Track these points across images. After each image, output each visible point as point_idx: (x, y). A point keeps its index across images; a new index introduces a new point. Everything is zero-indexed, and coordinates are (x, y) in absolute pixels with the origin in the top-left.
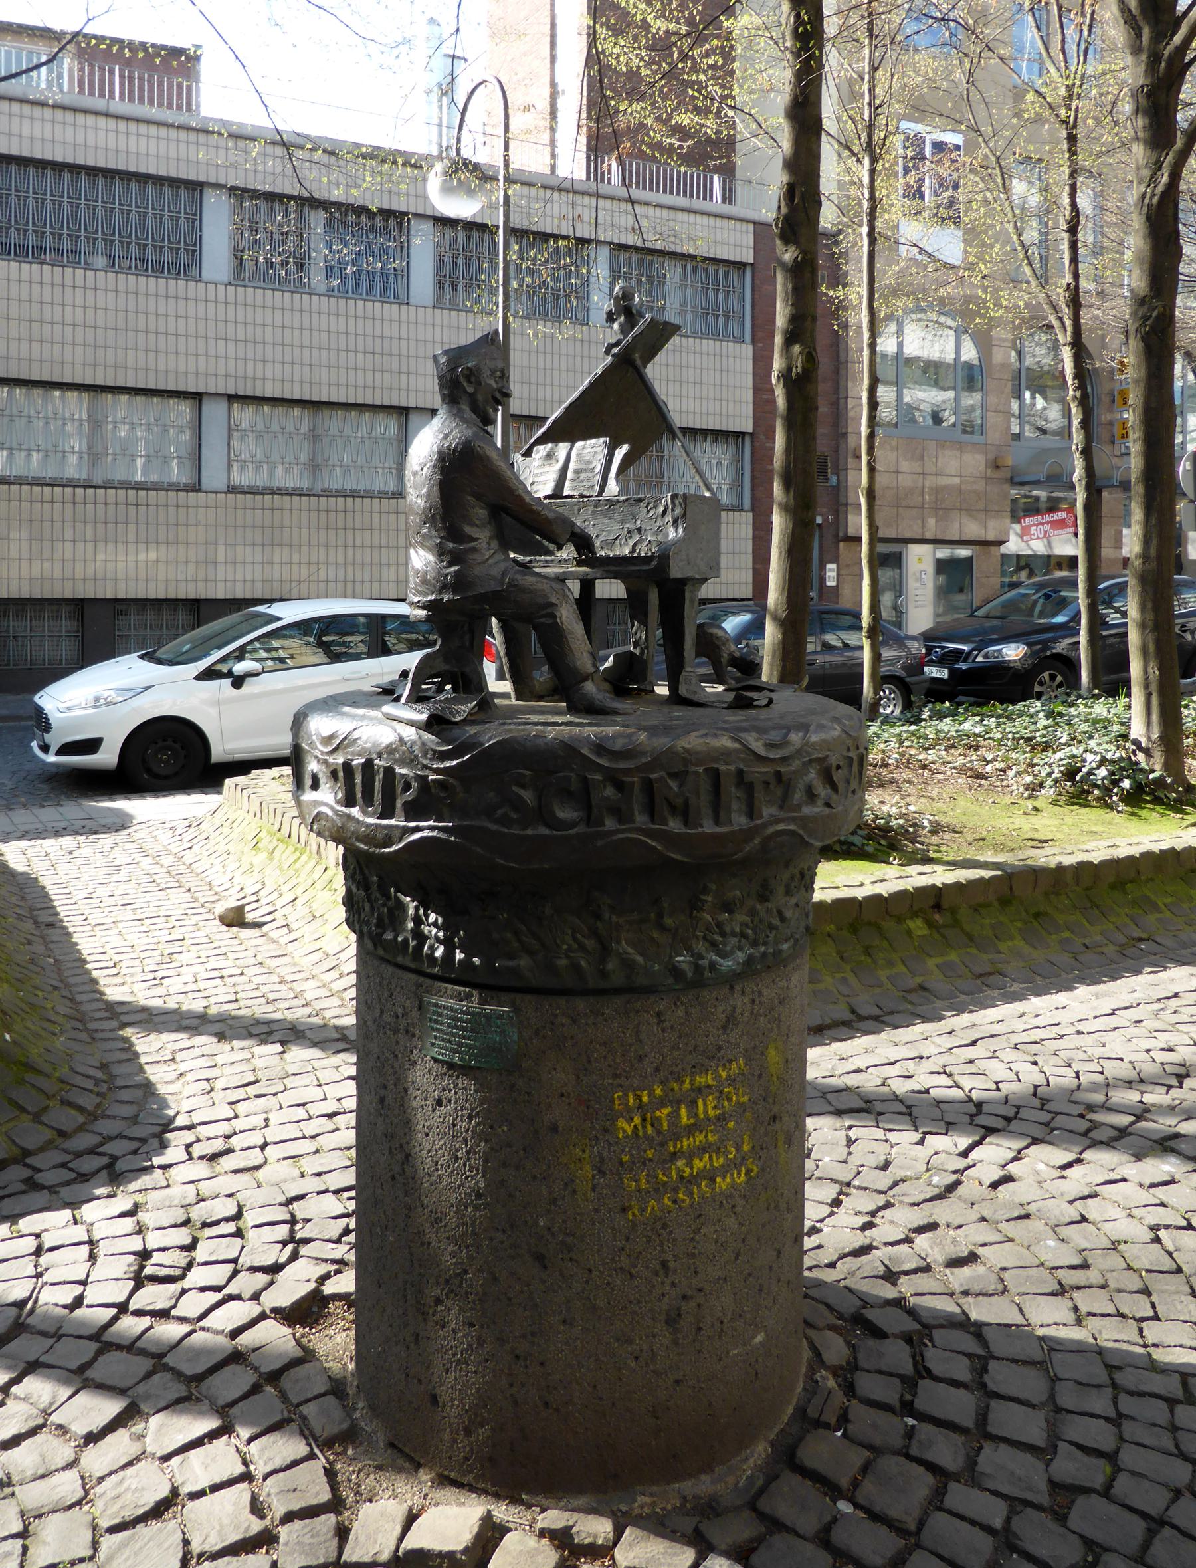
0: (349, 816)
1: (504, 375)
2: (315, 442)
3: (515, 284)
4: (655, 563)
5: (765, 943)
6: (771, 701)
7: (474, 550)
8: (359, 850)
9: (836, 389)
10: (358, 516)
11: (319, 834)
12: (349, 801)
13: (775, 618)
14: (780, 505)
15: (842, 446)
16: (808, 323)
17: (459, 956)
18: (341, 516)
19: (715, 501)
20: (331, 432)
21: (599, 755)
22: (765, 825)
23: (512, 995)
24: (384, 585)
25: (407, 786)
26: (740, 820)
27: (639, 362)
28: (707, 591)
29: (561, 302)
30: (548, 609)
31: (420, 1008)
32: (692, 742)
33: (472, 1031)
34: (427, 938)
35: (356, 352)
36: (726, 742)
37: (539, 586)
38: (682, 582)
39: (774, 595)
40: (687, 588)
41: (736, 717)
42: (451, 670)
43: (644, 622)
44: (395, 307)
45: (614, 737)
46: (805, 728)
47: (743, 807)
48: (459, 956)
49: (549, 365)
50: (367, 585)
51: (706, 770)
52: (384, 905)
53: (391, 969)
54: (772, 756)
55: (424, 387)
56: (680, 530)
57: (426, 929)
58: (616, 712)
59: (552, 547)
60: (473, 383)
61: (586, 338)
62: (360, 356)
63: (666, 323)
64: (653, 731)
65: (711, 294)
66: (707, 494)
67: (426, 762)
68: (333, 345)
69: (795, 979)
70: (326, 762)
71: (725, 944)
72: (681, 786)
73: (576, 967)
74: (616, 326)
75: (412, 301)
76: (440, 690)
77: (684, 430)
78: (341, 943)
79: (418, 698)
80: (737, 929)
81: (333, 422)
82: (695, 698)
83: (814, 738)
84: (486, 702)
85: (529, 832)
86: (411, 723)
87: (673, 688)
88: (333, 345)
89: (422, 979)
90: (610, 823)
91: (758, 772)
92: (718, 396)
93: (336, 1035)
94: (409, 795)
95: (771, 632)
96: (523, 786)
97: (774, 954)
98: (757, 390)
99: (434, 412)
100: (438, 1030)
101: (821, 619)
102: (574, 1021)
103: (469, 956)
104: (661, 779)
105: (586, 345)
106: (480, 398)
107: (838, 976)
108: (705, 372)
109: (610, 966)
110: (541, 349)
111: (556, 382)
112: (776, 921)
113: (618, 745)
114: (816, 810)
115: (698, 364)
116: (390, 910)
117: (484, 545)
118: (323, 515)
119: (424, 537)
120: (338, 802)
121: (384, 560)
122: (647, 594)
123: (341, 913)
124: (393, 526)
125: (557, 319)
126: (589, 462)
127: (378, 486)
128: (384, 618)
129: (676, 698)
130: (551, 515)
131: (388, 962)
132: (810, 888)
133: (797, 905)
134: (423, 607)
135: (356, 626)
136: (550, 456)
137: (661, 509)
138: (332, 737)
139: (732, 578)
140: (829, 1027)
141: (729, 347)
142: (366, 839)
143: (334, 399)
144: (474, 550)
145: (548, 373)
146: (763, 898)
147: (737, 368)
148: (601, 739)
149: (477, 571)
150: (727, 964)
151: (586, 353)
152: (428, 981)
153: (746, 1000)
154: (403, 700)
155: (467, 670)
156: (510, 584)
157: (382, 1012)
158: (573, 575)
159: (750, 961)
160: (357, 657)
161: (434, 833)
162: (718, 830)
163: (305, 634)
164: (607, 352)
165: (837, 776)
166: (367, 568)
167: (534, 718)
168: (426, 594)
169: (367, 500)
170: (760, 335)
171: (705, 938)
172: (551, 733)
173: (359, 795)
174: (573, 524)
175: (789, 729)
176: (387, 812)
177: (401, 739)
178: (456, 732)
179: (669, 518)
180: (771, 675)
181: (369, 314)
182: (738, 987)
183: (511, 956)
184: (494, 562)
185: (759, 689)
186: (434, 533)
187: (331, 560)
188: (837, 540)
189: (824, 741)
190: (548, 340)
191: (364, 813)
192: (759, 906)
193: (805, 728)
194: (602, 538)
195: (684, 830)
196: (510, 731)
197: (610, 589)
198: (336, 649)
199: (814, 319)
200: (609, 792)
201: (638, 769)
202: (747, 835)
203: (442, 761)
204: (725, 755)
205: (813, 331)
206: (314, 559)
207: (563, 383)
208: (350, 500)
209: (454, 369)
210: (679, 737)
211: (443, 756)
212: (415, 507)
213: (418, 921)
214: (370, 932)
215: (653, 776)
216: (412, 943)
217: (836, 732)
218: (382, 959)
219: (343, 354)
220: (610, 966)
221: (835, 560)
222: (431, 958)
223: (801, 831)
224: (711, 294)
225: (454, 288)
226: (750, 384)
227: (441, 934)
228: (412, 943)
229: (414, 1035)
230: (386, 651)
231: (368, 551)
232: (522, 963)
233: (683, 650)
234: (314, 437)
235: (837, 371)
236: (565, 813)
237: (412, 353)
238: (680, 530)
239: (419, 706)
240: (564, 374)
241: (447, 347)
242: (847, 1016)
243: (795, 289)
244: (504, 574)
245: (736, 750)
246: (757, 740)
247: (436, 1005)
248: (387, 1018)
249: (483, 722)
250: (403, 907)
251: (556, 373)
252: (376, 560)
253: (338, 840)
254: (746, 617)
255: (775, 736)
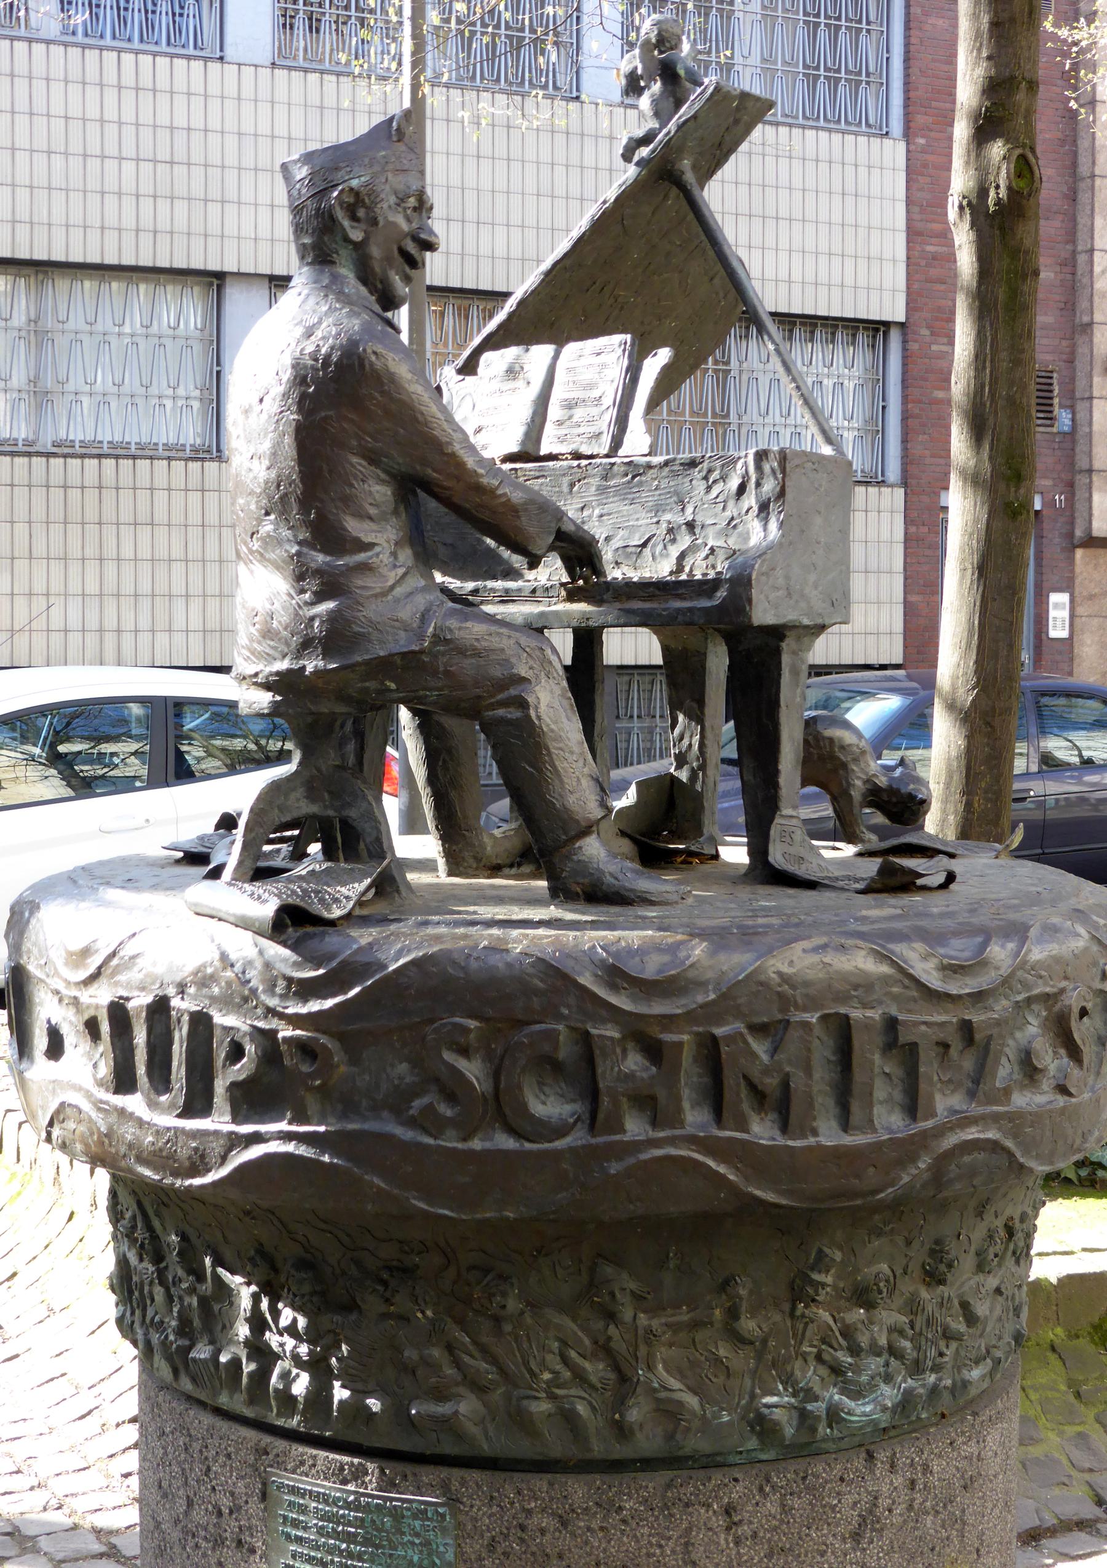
0: (122, 1112)
1: (423, 206)
2: (40, 346)
3: (433, 17)
4: (722, 593)
5: (936, 1368)
6: (951, 878)
7: (365, 568)
8: (143, 1181)
9: (1071, 235)
10: (126, 496)
11: (64, 1146)
12: (124, 1082)
13: (951, 706)
14: (963, 473)
15: (1083, 350)
16: (1021, 96)
17: (340, 1393)
18: (92, 495)
19: (841, 463)
20: (71, 325)
21: (613, 987)
22: (940, 1132)
23: (444, 1472)
24: (179, 638)
25: (236, 1052)
26: (889, 1121)
27: (689, 177)
28: (822, 651)
29: (525, 52)
30: (511, 690)
31: (264, 1496)
32: (797, 961)
33: (366, 1542)
34: (278, 1357)
35: (103, 157)
36: (862, 962)
37: (495, 642)
38: (777, 633)
39: (952, 662)
40: (787, 646)
41: (884, 910)
42: (328, 817)
43: (697, 716)
44: (197, 65)
45: (642, 952)
46: (1018, 932)
47: (898, 1095)
48: (340, 1393)
49: (501, 185)
50: (145, 638)
51: (824, 1018)
52: (192, 1290)
53: (208, 1419)
54: (954, 991)
55: (263, 232)
56: (773, 525)
57: (273, 1339)
58: (645, 900)
59: (517, 561)
60: (359, 223)
61: (575, 127)
62: (129, 167)
63: (745, 96)
64: (719, 938)
65: (822, 34)
66: (827, 450)
67: (273, 1002)
68: (76, 147)
69: (993, 1439)
70: (75, 1002)
71: (858, 1370)
72: (774, 1051)
73: (569, 1418)
74: (645, 102)
75: (230, 53)
76: (299, 854)
77: (788, 321)
78: (115, 1369)
79: (260, 873)
80: (883, 1341)
81: (75, 303)
82: (802, 871)
83: (1037, 954)
84: (388, 883)
85: (476, 1144)
86: (244, 923)
87: (758, 850)
88: (76, 147)
89: (267, 1439)
90: (635, 1127)
91: (925, 1023)
92: (837, 248)
93: (97, 1548)
94: (241, 1070)
95: (945, 736)
96: (464, 1052)
97: (953, 1390)
98: (913, 234)
99: (279, 283)
100: (299, 1540)
101: (1039, 708)
102: (564, 1523)
103: (360, 1393)
104: (731, 1039)
105: (575, 141)
106: (375, 251)
107: (1071, 1430)
108: (810, 197)
109: (634, 1415)
110: (486, 150)
111: (515, 219)
112: (958, 1325)
113: (651, 968)
114: (1040, 1099)
115: (797, 183)
116: (204, 1302)
117: (385, 558)
118: (57, 494)
119: (267, 541)
120: (100, 1083)
121: (178, 588)
122: (702, 656)
123: (108, 1305)
124: (195, 518)
125: (517, 87)
126: (591, 386)
127: (165, 435)
128: (178, 706)
129: (765, 872)
130: (517, 497)
131: (202, 1404)
132: (1023, 1256)
133: (998, 1291)
134: (267, 686)
135: (124, 721)
136: (512, 372)
137: (734, 483)
138: (86, 953)
139: (871, 627)
140: (1051, 1532)
141: (860, 146)
142: (159, 1159)
143: (76, 257)
144: (365, 568)
145: (500, 199)
146: (934, 1278)
147: (875, 191)
148: (617, 955)
149: (372, 611)
150: (861, 1410)
151: (575, 160)
152: (281, 1444)
153: (898, 1481)
154: (227, 874)
155: (353, 813)
156: (437, 639)
157: (190, 1503)
158: (560, 620)
159: (906, 1403)
160: (126, 785)
161: (290, 1147)
162: (848, 1140)
163: (24, 739)
164: (627, 156)
165: (1082, 1031)
166: (145, 604)
167: (486, 912)
168: (270, 659)
169: (143, 464)
170: (920, 119)
171: (819, 1358)
172: (519, 942)
173: (141, 1070)
174: (560, 515)
175: (987, 935)
176: (197, 1102)
177: (226, 961)
178: (332, 940)
179: (750, 500)
180: (943, 821)
181: (146, 81)
182: (882, 1456)
183: (440, 1395)
184: (402, 593)
185: (927, 852)
186: (286, 533)
187: (75, 587)
188: (1072, 545)
189: (1057, 960)
190: (500, 132)
191: (152, 1105)
192: (924, 1294)
193: (1018, 932)
194: (617, 543)
195: (781, 1141)
196: (438, 938)
197: (631, 646)
198: (86, 769)
199: (1032, 86)
200: (634, 1062)
201: (690, 1017)
202: (906, 1150)
203: (305, 1000)
204: (861, 988)
205: (1029, 114)
206: (39, 587)
207: (531, 221)
208: (109, 463)
209: (323, 193)
210: (770, 951)
211: (305, 990)
212: (247, 478)
213: (258, 1324)
214: (165, 1344)
215: (719, 1031)
216: (248, 1367)
217: (1079, 941)
218: (189, 1398)
219: (94, 164)
220: (634, 1415)
221: (1067, 585)
222: (286, 1399)
223: (1009, 1144)
224: (822, 34)
225: (314, 25)
226: (901, 223)
227: (303, 1349)
228: (248, 1367)
229: (252, 1551)
230: (183, 773)
231: (145, 568)
232: (463, 1408)
233: (776, 772)
234: (38, 334)
235: (1072, 197)
236: (549, 1106)
237: (231, 160)
238: (773, 525)
239: (258, 888)
240: (531, 201)
241: (313, 146)
242: (1090, 1511)
243: (995, 25)
244: (424, 618)
245: (885, 980)
246: (925, 958)
247: (294, 1490)
248: (199, 1515)
249: (384, 921)
250: (225, 1293)
251: (516, 200)
252: (161, 587)
253: (96, 1160)
254: (888, 705)
255: (959, 949)
